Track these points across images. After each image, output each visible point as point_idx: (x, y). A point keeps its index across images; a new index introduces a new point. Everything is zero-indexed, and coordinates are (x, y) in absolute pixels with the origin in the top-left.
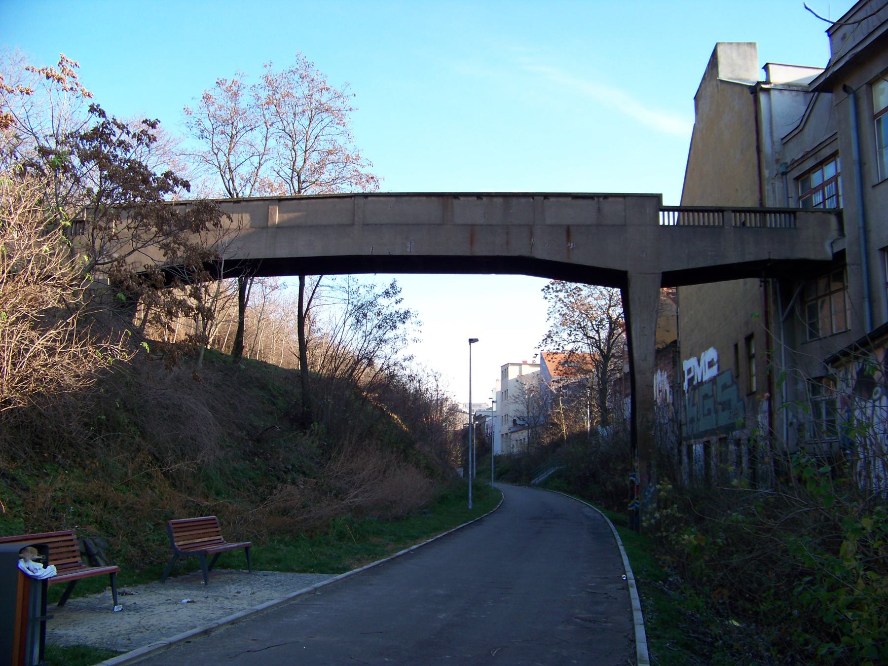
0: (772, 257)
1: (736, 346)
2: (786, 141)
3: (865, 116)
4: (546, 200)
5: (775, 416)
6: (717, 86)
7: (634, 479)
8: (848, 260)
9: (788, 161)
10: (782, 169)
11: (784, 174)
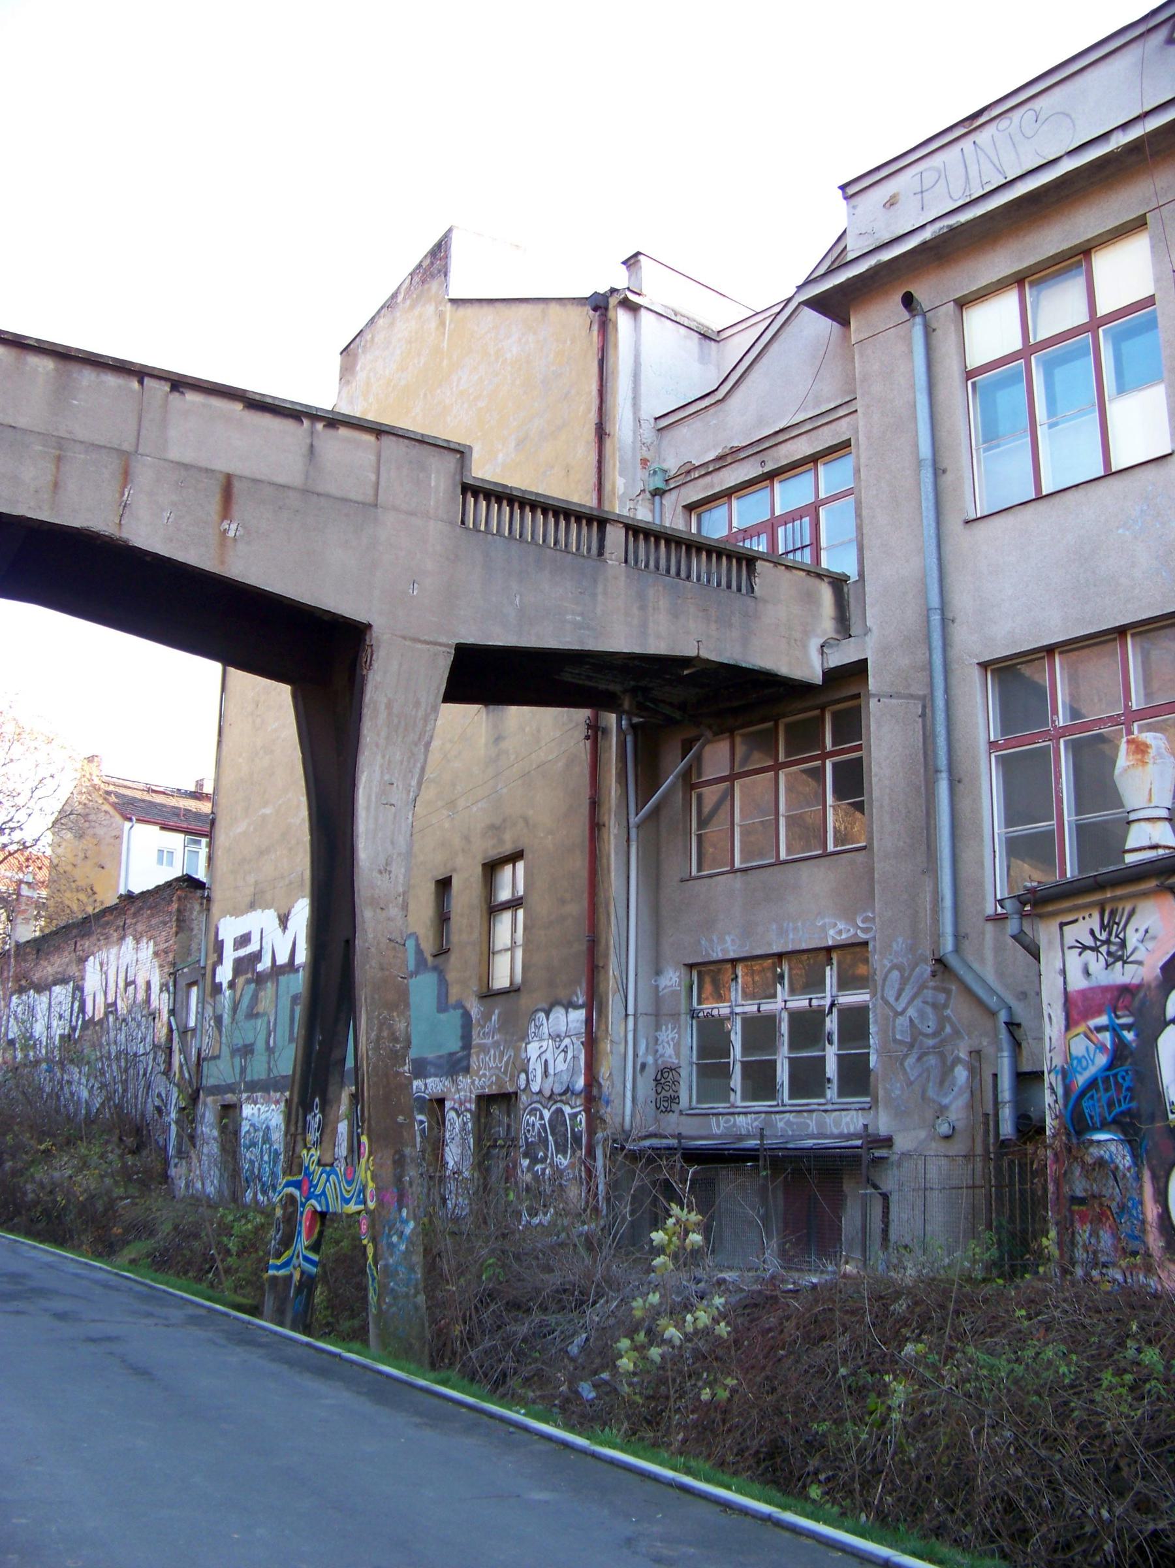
0: (704, 654)
1: (444, 885)
2: (666, 423)
3: (950, 372)
4: (176, 395)
5: (606, 1046)
6: (441, 316)
7: (297, 1193)
8: (873, 684)
9: (672, 465)
10: (658, 482)
11: (658, 493)
